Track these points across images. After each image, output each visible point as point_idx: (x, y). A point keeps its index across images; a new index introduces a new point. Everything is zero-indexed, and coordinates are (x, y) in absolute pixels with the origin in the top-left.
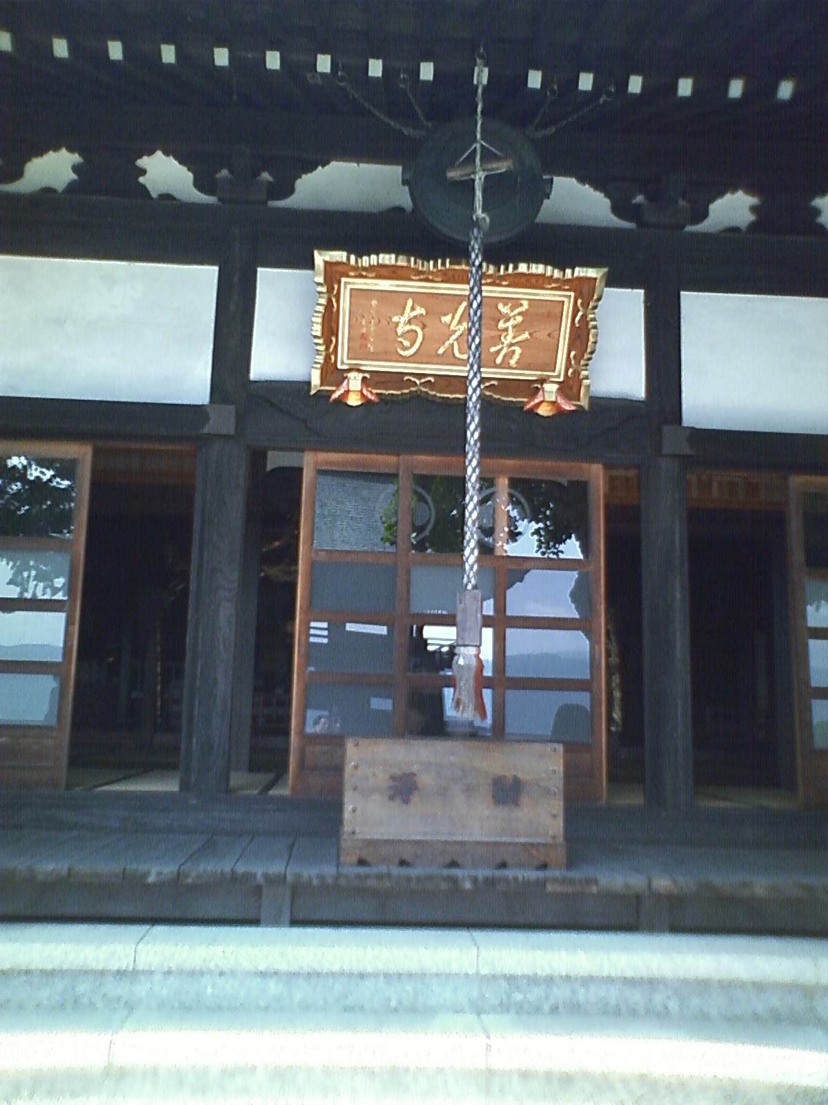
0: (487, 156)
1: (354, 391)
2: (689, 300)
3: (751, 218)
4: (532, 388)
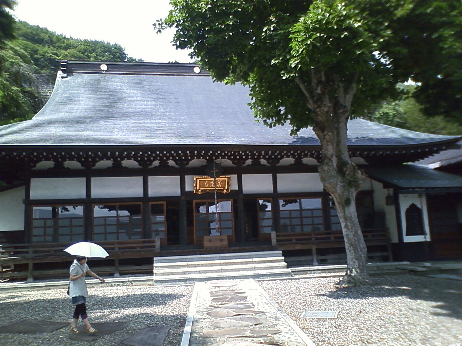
0: (215, 170)
1: (200, 192)
2: (278, 175)
3: (251, 163)
4: (223, 190)
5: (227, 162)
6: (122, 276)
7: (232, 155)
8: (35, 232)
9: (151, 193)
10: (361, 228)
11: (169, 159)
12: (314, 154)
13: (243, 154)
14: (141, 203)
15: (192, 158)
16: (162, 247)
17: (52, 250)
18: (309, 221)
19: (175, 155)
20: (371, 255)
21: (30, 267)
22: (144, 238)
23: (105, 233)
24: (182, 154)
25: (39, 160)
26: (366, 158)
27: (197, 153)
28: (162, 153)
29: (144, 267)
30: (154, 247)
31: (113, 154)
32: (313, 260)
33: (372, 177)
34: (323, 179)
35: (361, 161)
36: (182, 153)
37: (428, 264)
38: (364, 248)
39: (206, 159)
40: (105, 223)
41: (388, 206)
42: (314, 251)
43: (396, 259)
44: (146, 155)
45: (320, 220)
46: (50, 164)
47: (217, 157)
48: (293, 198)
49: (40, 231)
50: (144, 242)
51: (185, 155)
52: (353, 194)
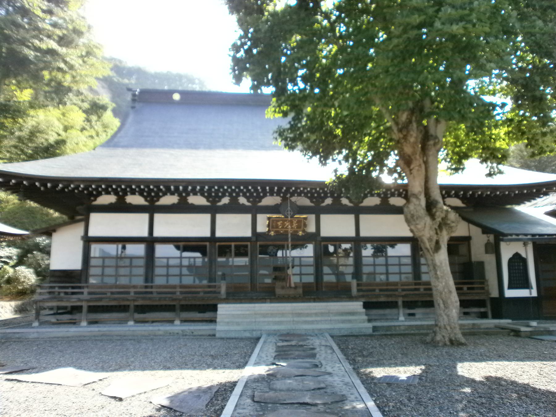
5: (305, 202)
6: (42, 326)
7: (308, 192)
8: (92, 271)
9: (219, 234)
10: (454, 278)
11: (239, 196)
12: (144, 190)
13: (321, 191)
14: (208, 244)
15: (265, 196)
16: (228, 294)
17: (109, 292)
18: (395, 269)
19: (245, 190)
20: (466, 310)
21: (85, 309)
22: (465, 279)
23: (168, 275)
24: (70, 188)
25: (99, 194)
26: (463, 199)
27: (277, 190)
28: (231, 188)
29: (208, 315)
30: (219, 293)
31: (177, 189)
32: (399, 314)
33: (470, 221)
34: (408, 221)
35: (457, 202)
36: (293, 190)
37: (534, 324)
38: (456, 302)
39: (281, 197)
40: (302, 266)
41: (488, 255)
42: (400, 304)
43: (494, 317)
44: (221, 190)
45: (409, 269)
46: (111, 199)
47: (292, 195)
48: (301, 243)
49: (163, 271)
50: (209, 287)
51: (256, 190)
52: (445, 238)
